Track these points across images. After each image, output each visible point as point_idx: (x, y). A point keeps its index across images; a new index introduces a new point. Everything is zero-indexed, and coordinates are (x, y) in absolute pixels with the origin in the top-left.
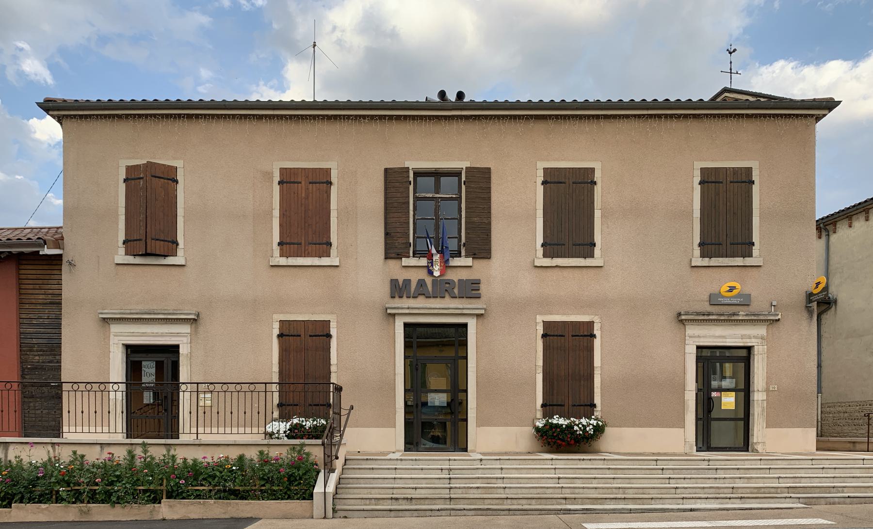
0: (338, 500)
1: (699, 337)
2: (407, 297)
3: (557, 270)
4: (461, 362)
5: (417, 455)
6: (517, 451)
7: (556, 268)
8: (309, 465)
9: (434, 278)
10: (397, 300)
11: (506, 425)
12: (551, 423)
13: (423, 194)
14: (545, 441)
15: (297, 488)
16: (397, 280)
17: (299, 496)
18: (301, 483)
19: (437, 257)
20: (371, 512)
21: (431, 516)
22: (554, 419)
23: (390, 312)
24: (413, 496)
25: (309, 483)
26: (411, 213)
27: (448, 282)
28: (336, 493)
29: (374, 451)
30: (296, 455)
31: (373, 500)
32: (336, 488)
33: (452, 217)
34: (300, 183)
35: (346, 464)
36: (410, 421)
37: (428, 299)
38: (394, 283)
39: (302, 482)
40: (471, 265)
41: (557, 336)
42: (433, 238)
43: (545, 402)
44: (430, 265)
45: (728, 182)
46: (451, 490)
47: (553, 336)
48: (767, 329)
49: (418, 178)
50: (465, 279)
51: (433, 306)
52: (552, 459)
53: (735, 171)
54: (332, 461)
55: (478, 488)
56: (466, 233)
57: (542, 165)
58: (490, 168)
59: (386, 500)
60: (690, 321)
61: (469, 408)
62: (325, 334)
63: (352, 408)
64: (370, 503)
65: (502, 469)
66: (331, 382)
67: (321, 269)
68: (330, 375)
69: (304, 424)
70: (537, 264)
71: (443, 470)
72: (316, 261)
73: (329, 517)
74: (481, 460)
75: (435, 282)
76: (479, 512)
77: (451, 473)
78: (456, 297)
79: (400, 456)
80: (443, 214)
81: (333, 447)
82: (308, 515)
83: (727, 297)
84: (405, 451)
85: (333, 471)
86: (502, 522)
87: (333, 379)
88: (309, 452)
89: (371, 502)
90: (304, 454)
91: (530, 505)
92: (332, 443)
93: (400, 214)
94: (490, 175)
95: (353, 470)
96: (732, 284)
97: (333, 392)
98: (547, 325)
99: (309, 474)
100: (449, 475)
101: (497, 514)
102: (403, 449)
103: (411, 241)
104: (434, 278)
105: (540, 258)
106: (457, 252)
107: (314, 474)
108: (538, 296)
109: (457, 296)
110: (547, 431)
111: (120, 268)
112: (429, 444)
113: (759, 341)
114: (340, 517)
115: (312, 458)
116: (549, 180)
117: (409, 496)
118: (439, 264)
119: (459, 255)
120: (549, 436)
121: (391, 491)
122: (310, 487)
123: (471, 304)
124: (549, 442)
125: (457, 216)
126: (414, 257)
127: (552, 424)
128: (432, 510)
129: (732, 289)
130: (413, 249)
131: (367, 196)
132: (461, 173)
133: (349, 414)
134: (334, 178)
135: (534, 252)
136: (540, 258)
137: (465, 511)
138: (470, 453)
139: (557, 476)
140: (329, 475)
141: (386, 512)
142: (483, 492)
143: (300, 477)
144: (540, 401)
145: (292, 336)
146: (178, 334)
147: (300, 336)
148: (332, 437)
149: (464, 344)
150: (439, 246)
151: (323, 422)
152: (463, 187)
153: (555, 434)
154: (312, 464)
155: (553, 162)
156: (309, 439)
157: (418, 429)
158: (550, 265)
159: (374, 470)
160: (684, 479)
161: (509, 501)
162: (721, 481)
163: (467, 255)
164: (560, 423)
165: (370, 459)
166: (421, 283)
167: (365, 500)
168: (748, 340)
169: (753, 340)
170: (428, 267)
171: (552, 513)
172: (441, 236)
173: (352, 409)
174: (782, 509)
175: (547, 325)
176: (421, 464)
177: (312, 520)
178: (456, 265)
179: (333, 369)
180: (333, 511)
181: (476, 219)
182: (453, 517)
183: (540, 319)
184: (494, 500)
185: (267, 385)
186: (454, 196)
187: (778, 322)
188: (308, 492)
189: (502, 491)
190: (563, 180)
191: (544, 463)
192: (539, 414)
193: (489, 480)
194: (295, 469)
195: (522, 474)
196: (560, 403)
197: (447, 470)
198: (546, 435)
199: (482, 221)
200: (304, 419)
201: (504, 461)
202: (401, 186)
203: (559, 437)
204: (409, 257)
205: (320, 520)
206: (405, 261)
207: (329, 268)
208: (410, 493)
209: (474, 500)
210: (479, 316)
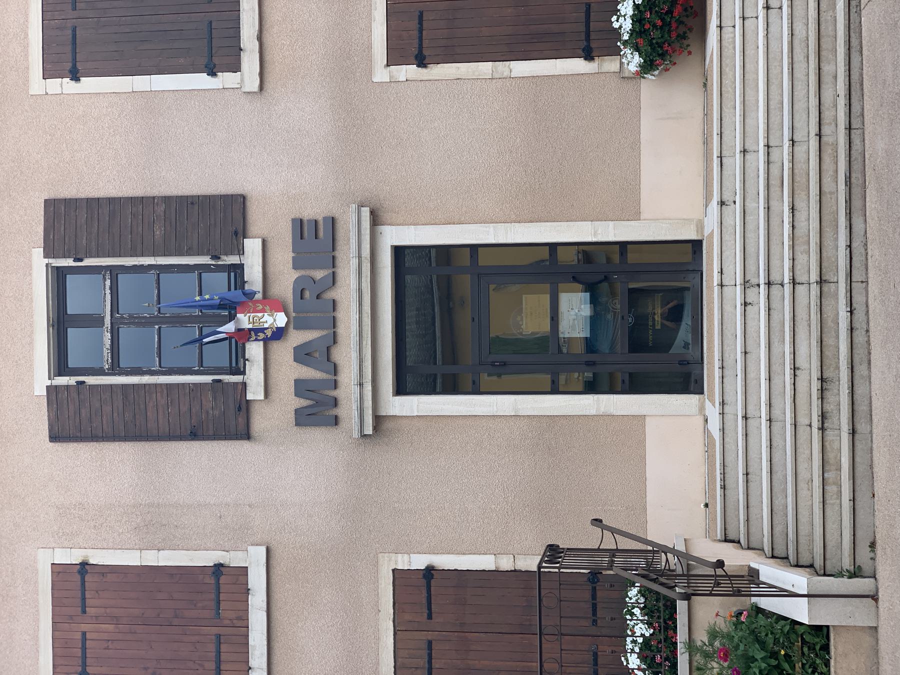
0: (828, 563)
2: (336, 388)
3: (268, 39)
4: (484, 260)
5: (711, 363)
6: (699, 113)
7: (264, 40)
8: (740, 634)
9: (292, 326)
10: (341, 412)
11: (636, 145)
12: (631, 35)
13: (105, 354)
14: (677, 46)
15: (798, 666)
16: (296, 411)
17: (818, 661)
18: (786, 655)
19: (244, 320)
20: (858, 482)
21: (867, 331)
22: (621, 27)
23: (371, 428)
24: (815, 374)
25: (787, 635)
26: (146, 379)
27: (300, 294)
28: (811, 566)
29: (703, 469)
30: (715, 665)
31: (826, 475)
32: (797, 566)
33: (155, 285)
34: (84, 634)
35: (737, 539)
36: (627, 381)
37: (340, 339)
38: (303, 418)
39: (783, 652)
40: (260, 240)
41: (421, 31)
42: (201, 330)
43: (580, 52)
44: (261, 336)
45: (75, 14)
46: (798, 280)
47: (421, 39)
49: (69, 312)
50: (291, 255)
51: (354, 328)
52: (720, 27)
54: (727, 576)
55: (793, 209)
56: (189, 253)
57: (37, 84)
58: (46, 201)
59: (827, 444)
61: (594, 240)
62: (424, 581)
63: (597, 522)
64: (834, 484)
65: (744, 151)
66: (535, 569)
67: (275, 588)
68: (520, 571)
69: (640, 640)
70: (255, 86)
71: (748, 301)
72: (257, 601)
73: (873, 587)
74: (722, 203)
75: (299, 323)
76: (856, 203)
77: (754, 281)
78: (334, 273)
79: (714, 405)
80: (148, 309)
81: (693, 572)
82: (867, 639)
84: (701, 392)
85: (753, 574)
86: (881, 145)
87: (530, 563)
88: (708, 633)
89: (831, 481)
90: (711, 645)
91: (836, 77)
92: (683, 575)
93: (150, 405)
94: (60, 200)
95: (751, 523)
97: (559, 568)
98: (395, 57)
99: (763, 634)
100: (759, 285)
101: (860, 159)
102: (697, 396)
103: (208, 379)
104: (292, 326)
105: (242, 80)
106: (232, 274)
107: (761, 619)
108: (328, 79)
109: (330, 271)
110: (651, 45)
112: (684, 333)
114: (873, 559)
115: (723, 625)
116: (69, 65)
117: (816, 385)
118: (260, 315)
119: (238, 269)
120: (662, 37)
121: (803, 431)
122: (796, 633)
123: (349, 240)
124: (678, 36)
125: (152, 275)
126: (243, 373)
127: (632, 32)
128: (852, 329)
130: (227, 374)
131: (111, 481)
132: (57, 268)
133: (613, 531)
134: (73, 557)
135: (227, 93)
136: (242, 80)
137: (854, 245)
138: (706, 235)
139: (761, 13)
140: (764, 583)
141: (857, 443)
142: (803, 195)
143: (770, 657)
144: (577, 65)
145: (430, 662)
147: (430, 643)
148: (669, 573)
149: (445, 252)
150: (219, 316)
151: (633, 592)
152: (88, 262)
153: (659, 23)
154: (737, 624)
155: (30, 59)
156: (676, 627)
157: (646, 362)
158: (258, 55)
159: (750, 470)
161: (826, 130)
163: (239, 251)
164: (630, 12)
165: (724, 479)
166: (303, 355)
167: (827, 496)
170: (266, 341)
171: (857, 21)
172: (197, 312)
173: (601, 521)
175: (395, 57)
176: (732, 356)
177: (880, 630)
178: (261, 275)
179: (506, 564)
180: (857, 577)
181: (158, 233)
182: (870, 275)
183: (381, 74)
184: (824, 167)
186: (108, 282)
188: (807, 638)
189: (800, 150)
190: (69, 32)
191: (731, 47)
192: (610, 65)
193: (772, 182)
194: (750, 667)
195: (758, 101)
196: (583, 15)
197: (748, 291)
198: (660, 46)
199: (163, 217)
200: (629, 639)
201: (723, 146)
202: (87, 405)
203: (667, 13)
204: (244, 385)
205: (881, 610)
206: (255, 393)
207: (272, 571)
208: (806, 384)
209: (824, 218)
210: (376, 220)
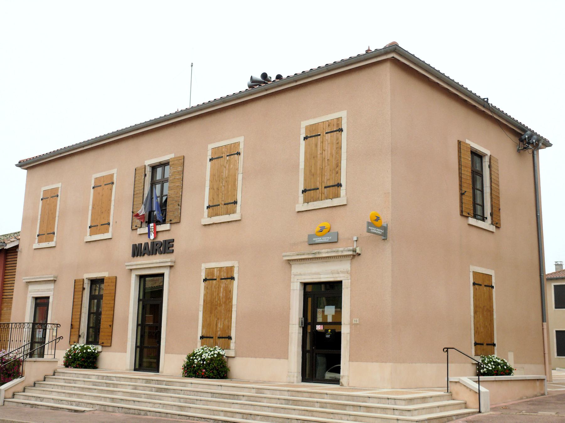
1: (300, 274)
48: (351, 264)
53: (329, 123)
96: (322, 224)
113: (346, 275)
146: (49, 290)
162: (300, 412)
168: (337, 275)
169: (341, 275)
187: (360, 257)
210: (171, 267)
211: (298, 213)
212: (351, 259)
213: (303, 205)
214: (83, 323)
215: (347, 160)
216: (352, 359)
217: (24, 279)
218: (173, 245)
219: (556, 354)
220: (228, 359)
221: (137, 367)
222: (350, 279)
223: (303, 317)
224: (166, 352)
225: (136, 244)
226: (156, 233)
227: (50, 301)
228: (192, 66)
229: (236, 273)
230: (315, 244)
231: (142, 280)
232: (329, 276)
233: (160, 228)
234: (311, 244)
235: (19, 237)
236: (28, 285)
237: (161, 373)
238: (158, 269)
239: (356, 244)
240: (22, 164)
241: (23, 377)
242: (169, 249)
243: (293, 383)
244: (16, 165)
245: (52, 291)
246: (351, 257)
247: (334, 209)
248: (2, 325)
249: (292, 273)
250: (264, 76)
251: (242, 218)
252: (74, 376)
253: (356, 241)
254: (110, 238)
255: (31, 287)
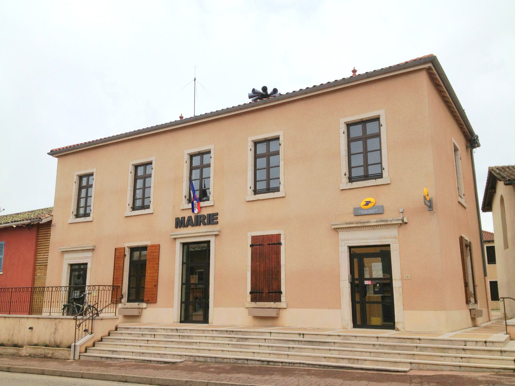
60: (344, 229)
83: (366, 209)
96: (368, 200)
111: (70, 225)
129: (367, 203)
146: (87, 258)
160: (330, 350)
174: (483, 368)
185: (100, 286)
187: (407, 225)
210: (216, 235)
211: (342, 191)
212: (398, 227)
213: (346, 185)
214: (125, 284)
215: (387, 148)
216: (406, 307)
217: (60, 249)
218: (217, 217)
219: (491, 300)
220: (142, 310)
221: (183, 319)
222: (399, 243)
223: (351, 274)
224: (215, 306)
225: (179, 218)
226: (200, 208)
227: (88, 267)
228: (195, 80)
229: (283, 239)
230: (361, 215)
231: (186, 247)
232: (376, 240)
233: (202, 204)
234: (357, 215)
235: (52, 214)
236: (64, 254)
237: (210, 324)
238: (203, 237)
239: (402, 215)
240: (53, 153)
241: (93, 334)
242: (213, 221)
243: (348, 329)
244: (47, 153)
245: (89, 258)
246: (399, 225)
247: (377, 187)
248: (6, 290)
249: (339, 239)
250: (265, 89)
251: (286, 195)
252: (185, 332)
253: (402, 212)
254: (151, 213)
255: (66, 256)
